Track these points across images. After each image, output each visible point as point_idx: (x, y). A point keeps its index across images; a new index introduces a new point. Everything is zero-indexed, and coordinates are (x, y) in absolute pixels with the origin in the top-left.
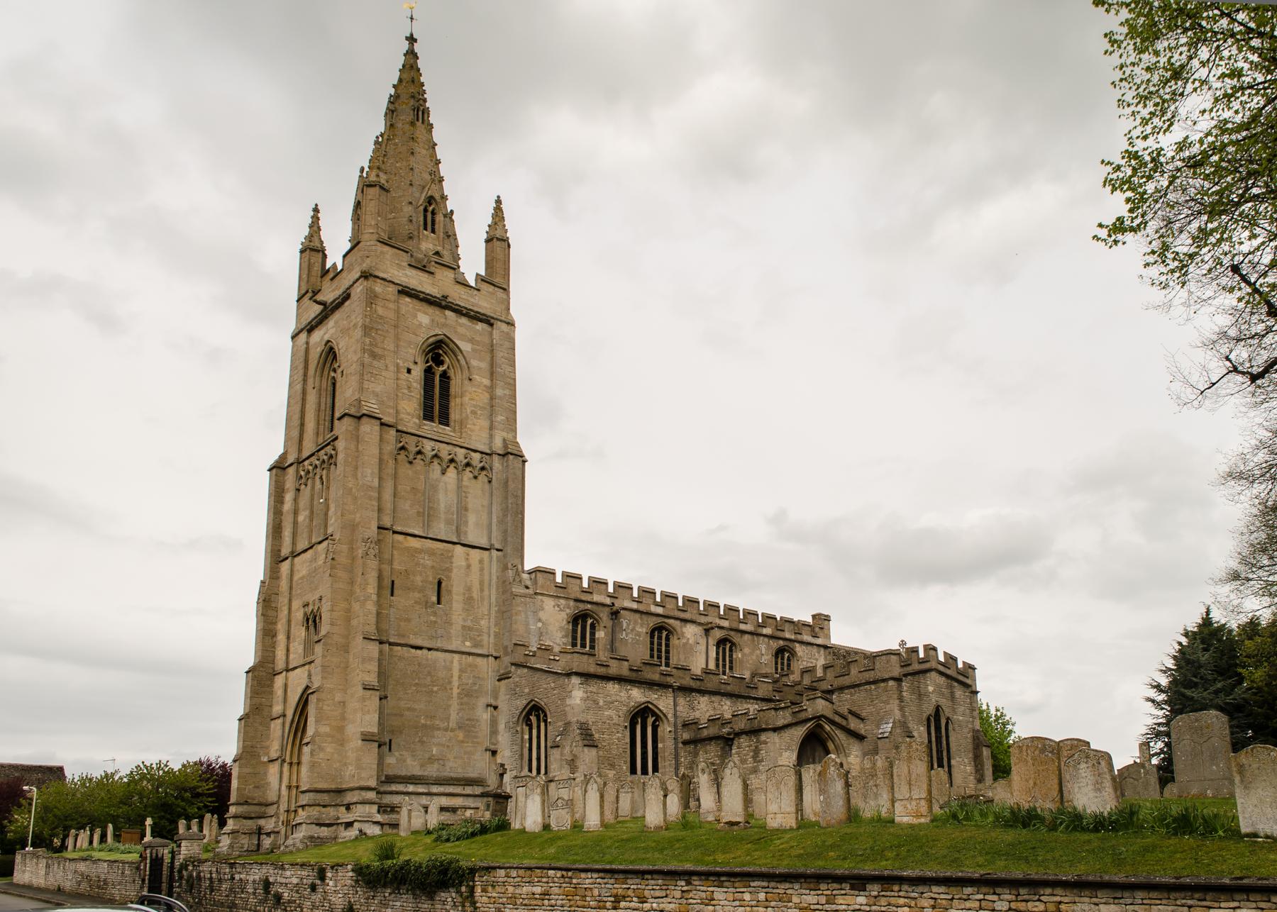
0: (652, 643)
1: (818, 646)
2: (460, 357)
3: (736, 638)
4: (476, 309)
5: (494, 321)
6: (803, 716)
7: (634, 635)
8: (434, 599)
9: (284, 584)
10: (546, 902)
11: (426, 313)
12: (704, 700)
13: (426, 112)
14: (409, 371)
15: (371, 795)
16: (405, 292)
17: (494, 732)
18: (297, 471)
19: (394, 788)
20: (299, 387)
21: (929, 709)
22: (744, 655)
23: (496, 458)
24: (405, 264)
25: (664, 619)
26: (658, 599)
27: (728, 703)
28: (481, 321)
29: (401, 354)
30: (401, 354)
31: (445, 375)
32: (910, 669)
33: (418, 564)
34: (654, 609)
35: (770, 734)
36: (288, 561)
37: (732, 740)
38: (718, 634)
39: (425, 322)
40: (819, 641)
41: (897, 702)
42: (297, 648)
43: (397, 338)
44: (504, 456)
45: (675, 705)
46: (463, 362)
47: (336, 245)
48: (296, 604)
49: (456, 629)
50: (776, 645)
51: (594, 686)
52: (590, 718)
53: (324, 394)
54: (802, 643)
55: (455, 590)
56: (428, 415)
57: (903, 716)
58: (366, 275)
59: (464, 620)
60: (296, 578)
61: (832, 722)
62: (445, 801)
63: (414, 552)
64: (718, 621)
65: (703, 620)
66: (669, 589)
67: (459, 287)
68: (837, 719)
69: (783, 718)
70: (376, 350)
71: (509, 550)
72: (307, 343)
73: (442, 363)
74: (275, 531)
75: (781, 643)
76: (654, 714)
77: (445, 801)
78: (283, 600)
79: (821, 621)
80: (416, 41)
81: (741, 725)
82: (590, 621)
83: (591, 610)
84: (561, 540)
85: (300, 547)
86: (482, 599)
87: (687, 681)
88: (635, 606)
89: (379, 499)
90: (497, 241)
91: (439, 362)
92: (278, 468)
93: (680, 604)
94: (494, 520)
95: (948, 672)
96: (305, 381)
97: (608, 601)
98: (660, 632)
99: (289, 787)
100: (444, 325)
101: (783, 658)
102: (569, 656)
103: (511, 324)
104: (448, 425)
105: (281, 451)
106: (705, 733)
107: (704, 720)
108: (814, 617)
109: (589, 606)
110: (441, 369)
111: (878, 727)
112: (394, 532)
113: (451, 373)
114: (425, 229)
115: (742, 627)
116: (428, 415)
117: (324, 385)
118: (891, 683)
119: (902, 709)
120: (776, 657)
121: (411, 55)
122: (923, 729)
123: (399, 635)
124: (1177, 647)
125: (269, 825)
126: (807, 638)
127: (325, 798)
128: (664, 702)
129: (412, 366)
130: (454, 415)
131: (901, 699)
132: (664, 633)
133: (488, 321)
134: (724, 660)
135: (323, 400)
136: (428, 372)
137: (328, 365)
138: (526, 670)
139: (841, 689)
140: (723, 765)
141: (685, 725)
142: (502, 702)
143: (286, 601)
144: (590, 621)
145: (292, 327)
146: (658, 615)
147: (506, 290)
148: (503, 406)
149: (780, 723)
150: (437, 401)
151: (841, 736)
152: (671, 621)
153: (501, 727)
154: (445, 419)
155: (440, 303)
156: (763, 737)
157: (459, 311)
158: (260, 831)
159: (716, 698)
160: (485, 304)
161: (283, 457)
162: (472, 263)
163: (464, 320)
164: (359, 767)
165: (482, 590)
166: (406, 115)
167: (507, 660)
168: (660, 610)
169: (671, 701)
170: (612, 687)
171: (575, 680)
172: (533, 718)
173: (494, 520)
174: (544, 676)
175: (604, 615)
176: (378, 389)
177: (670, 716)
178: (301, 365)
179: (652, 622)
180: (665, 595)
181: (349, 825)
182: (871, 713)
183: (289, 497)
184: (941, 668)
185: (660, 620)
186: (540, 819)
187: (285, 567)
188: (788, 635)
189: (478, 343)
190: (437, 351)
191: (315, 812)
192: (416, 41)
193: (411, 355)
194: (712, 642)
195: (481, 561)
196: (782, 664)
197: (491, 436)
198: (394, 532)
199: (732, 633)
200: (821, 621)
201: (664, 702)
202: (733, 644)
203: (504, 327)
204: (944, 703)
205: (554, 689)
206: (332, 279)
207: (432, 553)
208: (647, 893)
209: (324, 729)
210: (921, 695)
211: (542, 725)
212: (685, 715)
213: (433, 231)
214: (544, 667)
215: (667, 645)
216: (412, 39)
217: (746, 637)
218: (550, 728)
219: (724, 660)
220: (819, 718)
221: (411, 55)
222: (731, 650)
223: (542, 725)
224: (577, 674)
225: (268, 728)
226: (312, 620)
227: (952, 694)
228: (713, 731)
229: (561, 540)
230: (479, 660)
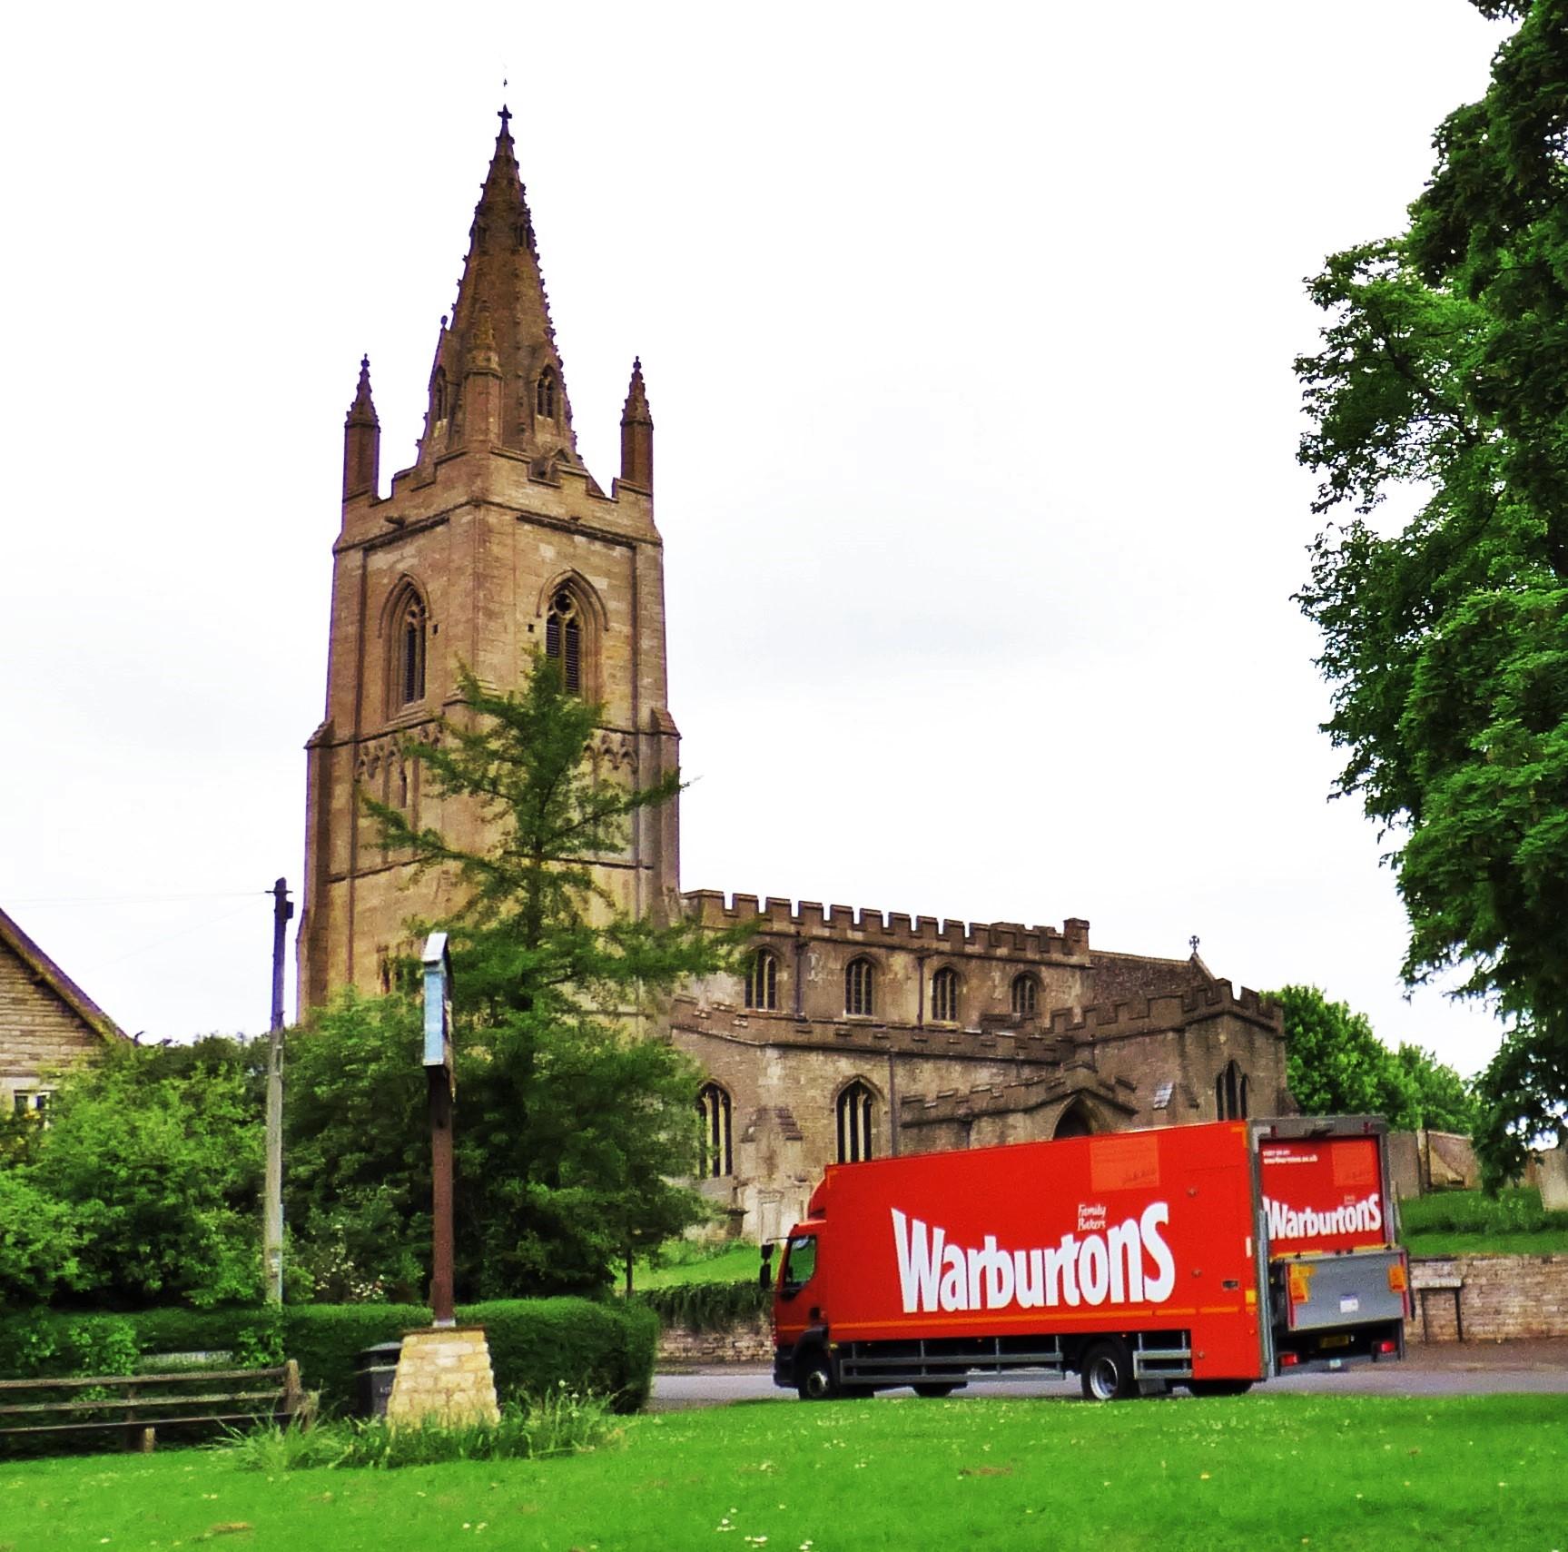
0: (848, 982)
1: (1073, 967)
2: (594, 599)
3: (960, 965)
4: (614, 530)
5: (639, 546)
6: (1060, 1090)
11: (550, 543)
12: (928, 1067)
14: (531, 628)
16: (527, 517)
18: (356, 755)
20: (352, 630)
21: (1220, 1066)
22: (970, 989)
23: (642, 738)
24: (524, 480)
26: (857, 921)
27: (958, 1068)
28: (620, 544)
31: (572, 624)
32: (1196, 1014)
34: (851, 935)
35: (1020, 1116)
36: (345, 883)
37: (970, 1123)
39: (549, 556)
40: (1074, 960)
41: (1178, 1061)
44: (652, 734)
45: (892, 1076)
46: (598, 606)
48: (360, 946)
50: (1013, 970)
51: (793, 1060)
52: (790, 1102)
53: (395, 645)
54: (1050, 964)
57: (1186, 1077)
60: (359, 908)
61: (1096, 1096)
64: (935, 945)
65: (916, 944)
66: (871, 905)
67: (591, 501)
68: (1102, 1092)
70: (491, 606)
71: (664, 868)
72: (364, 567)
76: (866, 1090)
79: (1077, 928)
80: (510, 116)
81: (981, 1104)
82: (768, 959)
87: (906, 1042)
88: (826, 933)
90: (636, 426)
92: (322, 747)
93: (886, 924)
94: (642, 826)
95: (1248, 1013)
96: (362, 621)
97: (792, 929)
98: (859, 968)
100: (574, 556)
101: (1023, 989)
102: (762, 1022)
105: (321, 718)
106: (933, 1113)
107: (931, 1096)
108: (1068, 923)
109: (768, 939)
110: (569, 616)
111: (1154, 1092)
115: (969, 949)
117: (395, 633)
118: (1170, 1035)
119: (1184, 1068)
120: (1015, 988)
121: (505, 140)
122: (1212, 1093)
124: (1494, 995)
126: (1057, 956)
128: (878, 1074)
129: (535, 621)
131: (1183, 1054)
132: (865, 968)
134: (944, 998)
135: (395, 655)
136: (552, 620)
137: (402, 605)
138: (695, 1036)
139: (1106, 1041)
141: (905, 1102)
143: (344, 939)
144: (768, 959)
146: (856, 943)
147: (650, 496)
149: (1033, 1101)
151: (1106, 1113)
152: (874, 950)
155: (567, 527)
156: (1011, 1119)
159: (943, 1064)
160: (625, 521)
162: (601, 456)
163: (598, 546)
168: (859, 936)
169: (886, 1072)
170: (815, 1059)
171: (772, 1054)
172: (707, 1101)
173: (642, 826)
174: (724, 1046)
175: (787, 949)
177: (886, 1091)
178: (352, 597)
179: (850, 952)
180: (865, 914)
182: (1146, 1075)
184: (1236, 1009)
185: (858, 949)
188: (1030, 955)
192: (510, 116)
194: (928, 973)
195: (626, 884)
196: (1023, 997)
197: (635, 708)
199: (955, 960)
200: (1077, 928)
201: (878, 1074)
203: (649, 549)
204: (1240, 1055)
205: (741, 1063)
210: (1209, 1048)
211: (722, 1110)
212: (903, 1088)
213: (550, 414)
214: (726, 1034)
215: (869, 984)
216: (505, 115)
217: (974, 963)
218: (734, 1115)
220: (1079, 1092)
221: (505, 140)
222: (953, 984)
223: (722, 1110)
224: (775, 1046)
227: (1251, 1042)
228: (945, 1110)
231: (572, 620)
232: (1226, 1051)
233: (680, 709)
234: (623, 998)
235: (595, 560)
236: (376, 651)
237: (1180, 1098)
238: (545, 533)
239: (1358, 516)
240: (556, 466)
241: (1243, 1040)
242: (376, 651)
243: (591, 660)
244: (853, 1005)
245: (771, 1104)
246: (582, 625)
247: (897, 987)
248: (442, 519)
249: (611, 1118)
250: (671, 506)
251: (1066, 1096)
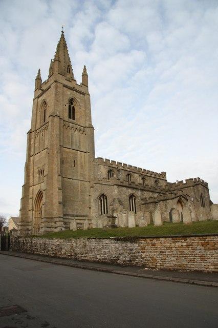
5: (85, 94)
7: (123, 176)
9: (32, 163)
13: (67, 47)
15: (62, 219)
16: (65, 86)
17: (90, 202)
19: (67, 217)
20: (35, 112)
21: (200, 194)
25: (131, 171)
29: (62, 103)
30: (62, 103)
31: (73, 108)
33: (69, 156)
35: (170, 200)
38: (142, 176)
42: (36, 180)
43: (63, 97)
47: (45, 77)
49: (79, 174)
51: (121, 188)
55: (78, 163)
56: (70, 117)
58: (56, 82)
60: (35, 161)
61: (183, 197)
62: (78, 221)
63: (67, 152)
69: (173, 196)
74: (29, 149)
76: (134, 196)
77: (78, 221)
78: (31, 167)
83: (113, 168)
84: (101, 151)
85: (36, 153)
88: (123, 168)
89: (60, 138)
90: (85, 75)
91: (72, 104)
92: (30, 133)
99: (35, 217)
103: (89, 95)
106: (149, 201)
113: (75, 107)
115: (147, 175)
121: (63, 35)
125: (30, 228)
126: (161, 178)
127: (49, 220)
130: (76, 117)
133: (84, 94)
136: (70, 106)
140: (155, 210)
142: (92, 194)
145: (33, 97)
148: (88, 116)
149: (173, 197)
150: (72, 113)
153: (92, 201)
154: (74, 118)
156: (168, 201)
157: (77, 91)
158: (28, 230)
161: (31, 130)
162: (79, 81)
164: (56, 211)
166: (61, 49)
167: (92, 182)
168: (128, 170)
170: (124, 189)
171: (115, 186)
172: (102, 198)
175: (116, 170)
176: (59, 109)
178: (36, 107)
179: (127, 173)
181: (56, 228)
183: (33, 140)
186: (134, 223)
187: (32, 158)
190: (71, 101)
191: (46, 224)
193: (66, 101)
201: (138, 193)
207: (72, 153)
209: (48, 201)
216: (63, 32)
221: (63, 35)
224: (116, 185)
225: (28, 201)
226: (41, 172)
228: (152, 201)
229: (101, 151)
230: (85, 182)
233: (93, 124)
235: (78, 96)
236: (39, 114)
237: (195, 200)
238: (69, 90)
240: (72, 79)
242: (39, 114)
244: (7, 240)
245: (116, 198)
249: (4, 226)
250: (92, 89)
251: (178, 197)
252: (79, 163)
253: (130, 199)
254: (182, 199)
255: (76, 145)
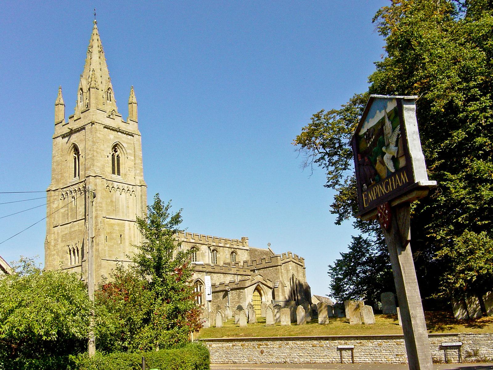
8: (120, 242)
10: (234, 348)
14: (108, 156)
39: (113, 137)
46: (125, 151)
56: (114, 173)
59: (129, 250)
61: (263, 284)
63: (112, 225)
73: (117, 152)
75: (233, 249)
86: (135, 240)
104: (120, 175)
112: (107, 218)
113: (120, 156)
114: (108, 100)
115: (220, 245)
116: (114, 173)
120: (231, 255)
123: (109, 256)
126: (241, 247)
154: (119, 173)
160: (131, 129)
165: (134, 237)
168: (193, 241)
188: (235, 247)
189: (129, 143)
198: (107, 218)
202: (217, 251)
206: (75, 121)
207: (118, 225)
208: (269, 343)
210: (288, 271)
219: (214, 258)
231: (118, 155)
232: (291, 271)
234: (64, 300)
239: (297, 144)
241: (295, 268)
243: (123, 166)
246: (121, 157)
247: (203, 255)
248: (83, 128)
252: (127, 237)
253: (231, 255)
254: (261, 285)
255: (123, 212)
